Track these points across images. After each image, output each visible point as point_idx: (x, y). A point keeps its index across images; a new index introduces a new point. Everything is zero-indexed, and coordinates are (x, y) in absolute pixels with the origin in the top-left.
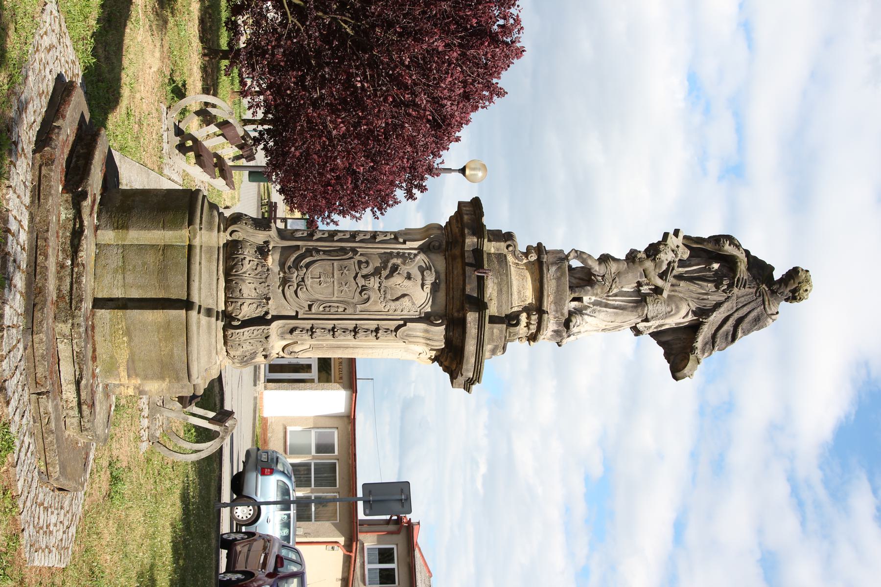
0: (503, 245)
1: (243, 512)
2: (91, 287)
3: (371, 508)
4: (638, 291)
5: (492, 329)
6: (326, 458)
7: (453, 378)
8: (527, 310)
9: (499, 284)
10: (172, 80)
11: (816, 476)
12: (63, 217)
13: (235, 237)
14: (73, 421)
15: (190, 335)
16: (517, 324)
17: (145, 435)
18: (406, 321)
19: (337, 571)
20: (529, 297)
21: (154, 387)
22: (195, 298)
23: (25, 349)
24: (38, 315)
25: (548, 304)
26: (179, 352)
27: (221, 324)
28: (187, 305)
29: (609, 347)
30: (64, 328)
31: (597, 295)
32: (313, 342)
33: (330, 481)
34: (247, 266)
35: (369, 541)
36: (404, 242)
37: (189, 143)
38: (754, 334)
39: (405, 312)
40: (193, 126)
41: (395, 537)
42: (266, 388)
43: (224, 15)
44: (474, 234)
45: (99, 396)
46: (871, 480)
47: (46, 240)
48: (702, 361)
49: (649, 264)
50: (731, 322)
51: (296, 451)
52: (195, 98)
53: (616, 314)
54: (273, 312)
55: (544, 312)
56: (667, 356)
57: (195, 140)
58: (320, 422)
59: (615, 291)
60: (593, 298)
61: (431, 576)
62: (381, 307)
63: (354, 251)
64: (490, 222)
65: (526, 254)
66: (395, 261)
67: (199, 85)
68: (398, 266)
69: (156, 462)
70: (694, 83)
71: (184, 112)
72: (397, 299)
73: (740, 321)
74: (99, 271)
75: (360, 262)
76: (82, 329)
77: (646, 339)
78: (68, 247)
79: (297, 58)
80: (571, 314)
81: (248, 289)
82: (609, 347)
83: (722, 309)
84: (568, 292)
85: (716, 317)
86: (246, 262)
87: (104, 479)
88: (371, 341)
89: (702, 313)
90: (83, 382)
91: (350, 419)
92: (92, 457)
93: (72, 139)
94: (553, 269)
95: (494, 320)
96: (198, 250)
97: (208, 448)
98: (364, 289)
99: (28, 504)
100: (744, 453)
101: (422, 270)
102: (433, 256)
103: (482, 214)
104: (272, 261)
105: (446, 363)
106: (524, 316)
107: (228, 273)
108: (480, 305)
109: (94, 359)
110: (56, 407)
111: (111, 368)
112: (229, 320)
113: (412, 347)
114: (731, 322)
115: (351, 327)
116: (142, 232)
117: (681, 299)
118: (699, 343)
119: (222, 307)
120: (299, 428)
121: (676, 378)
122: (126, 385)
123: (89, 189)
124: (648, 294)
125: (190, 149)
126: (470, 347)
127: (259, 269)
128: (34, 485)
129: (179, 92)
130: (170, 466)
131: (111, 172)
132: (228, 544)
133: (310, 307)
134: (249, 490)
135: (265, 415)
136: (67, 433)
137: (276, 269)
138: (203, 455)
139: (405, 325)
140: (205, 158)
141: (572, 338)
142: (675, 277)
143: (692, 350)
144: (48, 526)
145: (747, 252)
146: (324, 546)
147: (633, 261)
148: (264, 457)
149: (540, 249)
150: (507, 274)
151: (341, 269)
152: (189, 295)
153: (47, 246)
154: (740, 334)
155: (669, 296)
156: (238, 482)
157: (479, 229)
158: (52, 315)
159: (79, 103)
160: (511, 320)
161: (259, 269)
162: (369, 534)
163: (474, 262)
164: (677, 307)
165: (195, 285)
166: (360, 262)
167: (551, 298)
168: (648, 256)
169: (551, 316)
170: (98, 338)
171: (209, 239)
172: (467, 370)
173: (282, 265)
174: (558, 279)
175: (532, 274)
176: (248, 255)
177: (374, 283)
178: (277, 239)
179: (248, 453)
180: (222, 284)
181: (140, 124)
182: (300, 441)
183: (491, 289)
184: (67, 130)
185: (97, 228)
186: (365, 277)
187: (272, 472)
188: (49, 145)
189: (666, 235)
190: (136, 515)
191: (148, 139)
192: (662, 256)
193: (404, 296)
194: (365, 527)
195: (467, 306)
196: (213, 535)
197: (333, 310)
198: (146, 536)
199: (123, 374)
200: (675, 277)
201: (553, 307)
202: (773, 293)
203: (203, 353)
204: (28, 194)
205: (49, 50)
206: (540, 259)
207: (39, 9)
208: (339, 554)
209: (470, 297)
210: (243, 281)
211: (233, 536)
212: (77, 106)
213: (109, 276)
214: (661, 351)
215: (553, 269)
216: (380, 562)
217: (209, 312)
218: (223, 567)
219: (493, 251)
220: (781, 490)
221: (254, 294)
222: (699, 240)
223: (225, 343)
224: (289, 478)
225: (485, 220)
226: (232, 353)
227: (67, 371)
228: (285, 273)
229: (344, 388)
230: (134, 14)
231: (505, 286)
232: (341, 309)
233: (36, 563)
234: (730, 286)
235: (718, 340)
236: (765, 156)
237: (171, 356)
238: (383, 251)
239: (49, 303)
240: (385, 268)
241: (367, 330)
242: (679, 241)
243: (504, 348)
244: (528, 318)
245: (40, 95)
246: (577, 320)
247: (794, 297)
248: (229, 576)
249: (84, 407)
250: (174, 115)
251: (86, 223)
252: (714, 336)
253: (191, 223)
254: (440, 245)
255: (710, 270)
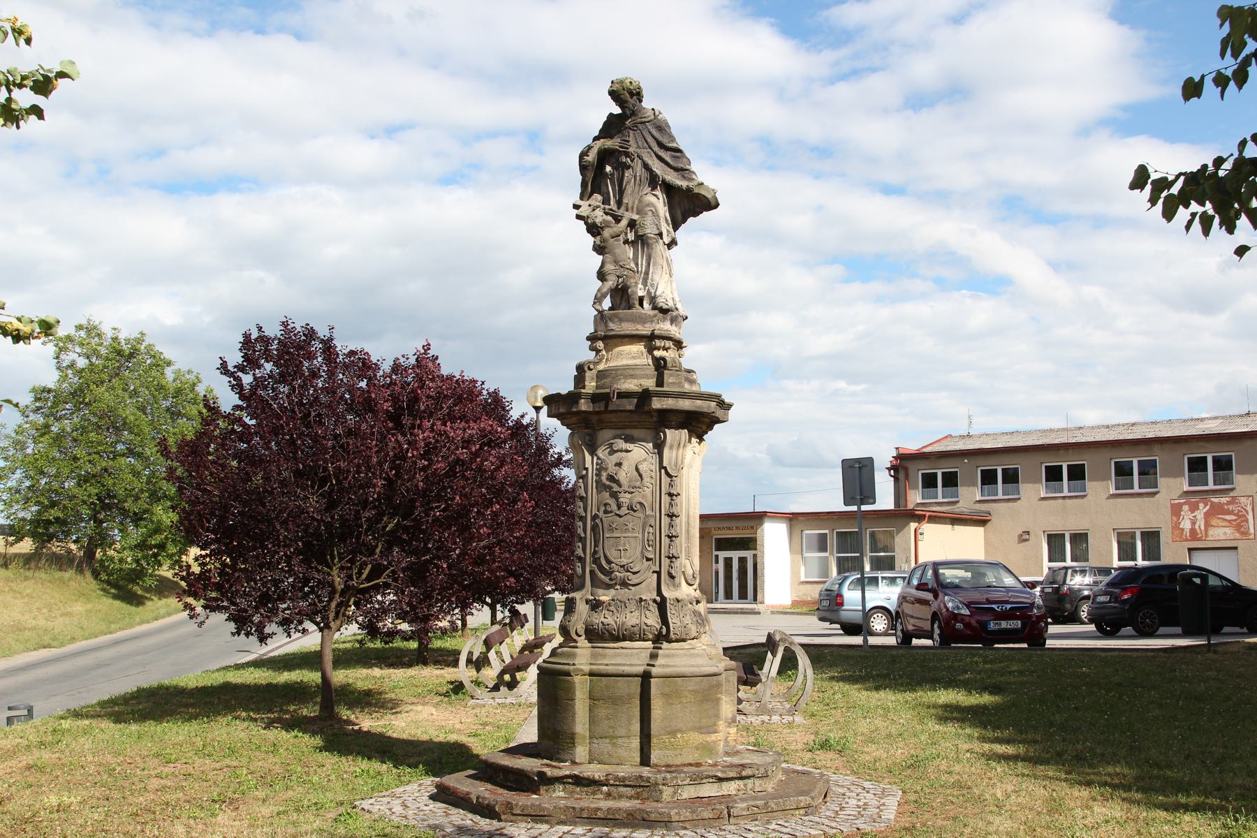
0: (588, 374)
1: (879, 623)
2: (629, 768)
3: (868, 497)
4: (633, 243)
5: (669, 384)
6: (832, 542)
7: (718, 421)
8: (650, 350)
9: (626, 377)
10: (446, 695)
11: (829, 56)
12: (562, 794)
13: (582, 632)
14: (759, 784)
15: (674, 674)
16: (664, 359)
17: (788, 718)
18: (662, 467)
19: (944, 530)
20: (639, 348)
21: (727, 708)
22: (640, 669)
23: (685, 828)
24: (653, 817)
25: (645, 330)
26: (692, 685)
27: (665, 645)
28: (646, 677)
29: (688, 267)
30: (667, 792)
31: (637, 283)
32: (683, 556)
33: (855, 535)
34: (610, 620)
35: (915, 497)
36: (586, 469)
37: (507, 677)
38: (674, 131)
39: (653, 468)
40: (490, 674)
41: (911, 472)
42: (762, 603)
43: (378, 644)
44: (577, 403)
45: (736, 760)
46: (828, 7)
47: (582, 810)
48: (700, 180)
49: (606, 233)
50: (662, 153)
51: (825, 572)
52: (463, 673)
53: (655, 264)
54: (654, 595)
55: (653, 333)
56: (696, 214)
57: (503, 672)
58: (796, 547)
59: (633, 265)
60: (640, 286)
61: (950, 436)
62: (648, 491)
63: (594, 517)
64: (567, 387)
65: (598, 351)
66: (604, 478)
67: (451, 670)
69: (815, 708)
70: (448, 180)
71: (477, 683)
72: (641, 476)
73: (661, 145)
74: (614, 761)
75: (606, 512)
76: (668, 776)
77: (681, 234)
78: (590, 789)
79: (418, 574)
80: (655, 308)
81: (631, 619)
82: (688, 267)
83: (650, 162)
84: (634, 310)
85: (658, 168)
86: (605, 621)
87: (823, 757)
88: (682, 501)
89: (654, 181)
90: (720, 774)
91: (794, 519)
92: (800, 768)
93: (489, 786)
94: (611, 325)
95: (660, 383)
96: (594, 667)
97: (803, 660)
98: (631, 508)
99: (834, 824)
100: (811, 128)
101: (612, 452)
102: (600, 441)
103: (559, 394)
104: (605, 596)
105: (704, 427)
106: (657, 353)
107: (617, 639)
108: (645, 396)
109: (698, 765)
110: (743, 800)
111: (709, 749)
112: (661, 637)
113: (687, 461)
114: (662, 153)
115: (668, 520)
116: (577, 720)
117: (640, 201)
118: (683, 184)
119: (649, 644)
120: (803, 569)
121: (717, 205)
122: (726, 735)
123: (535, 770)
124: (636, 233)
125: (513, 677)
126: (686, 404)
127: (612, 608)
128: (817, 819)
129: (458, 687)
130: (821, 695)
131: (524, 750)
132: (907, 638)
133: (648, 559)
134: (857, 617)
135: (789, 603)
136: (770, 790)
137: (612, 592)
138: (808, 662)
139: (665, 468)
140: (520, 662)
141: (679, 306)
142: (619, 208)
143: (689, 190)
144: (859, 807)
145: (596, 139)
146: (920, 543)
147: (604, 248)
148: (825, 603)
149: (592, 338)
150: (616, 369)
151: (611, 530)
152: (636, 676)
153: (588, 808)
154: (674, 145)
155: (638, 213)
156: (850, 629)
157: (573, 398)
158: (655, 804)
159: (456, 780)
160: (660, 366)
161: (612, 608)
164: (648, 205)
165: (628, 669)
166: (606, 512)
167: (639, 327)
168: (599, 234)
169: (657, 327)
170: (678, 761)
171: (583, 656)
172: (709, 407)
173: (608, 587)
174: (621, 320)
175: (617, 346)
176: (599, 619)
177: (625, 499)
178: (584, 591)
179: (821, 619)
180: (627, 644)
181: (485, 724)
182: (815, 568)
183: (631, 385)
184: (482, 790)
185: (574, 763)
186: (619, 507)
187: (840, 596)
188: (493, 807)
189: (578, 217)
190: (863, 726)
191: (501, 717)
192: (598, 221)
193: (637, 469)
194: (902, 502)
195: (646, 408)
196: (894, 652)
197: (652, 537)
198: (885, 716)
199: (713, 737)
200: (619, 208)
201: (647, 325)
202: (633, 114)
203: (693, 661)
204: (539, 826)
205: (405, 806)
206: (603, 338)
207: (367, 815)
208: (928, 528)
209: (637, 406)
210: (623, 623)
211: (899, 633)
212: (460, 781)
213: (620, 751)
214: (691, 220)
215: (611, 325)
216: (936, 486)
217: (654, 656)
218: (928, 642)
219: (594, 384)
220: (843, 90)
221: (636, 614)
222: (584, 185)
223: (684, 640)
224: (846, 578)
225: (564, 392)
226: (694, 634)
227: (709, 790)
229: (762, 524)
230: (379, 730)
231: (628, 372)
232: (651, 530)
233: (892, 817)
234: (627, 155)
235: (680, 165)
236: (515, 110)
237: (695, 692)
239: (642, 807)
240: (611, 488)
241: (671, 505)
242: (584, 204)
243: (689, 371)
244: (658, 349)
245: (448, 815)
246: (661, 302)
247: (637, 94)
248: (936, 636)
249: (744, 773)
250: (479, 692)
251: (567, 773)
252: (676, 169)
253: (568, 674)
254: (589, 435)
255: (612, 175)
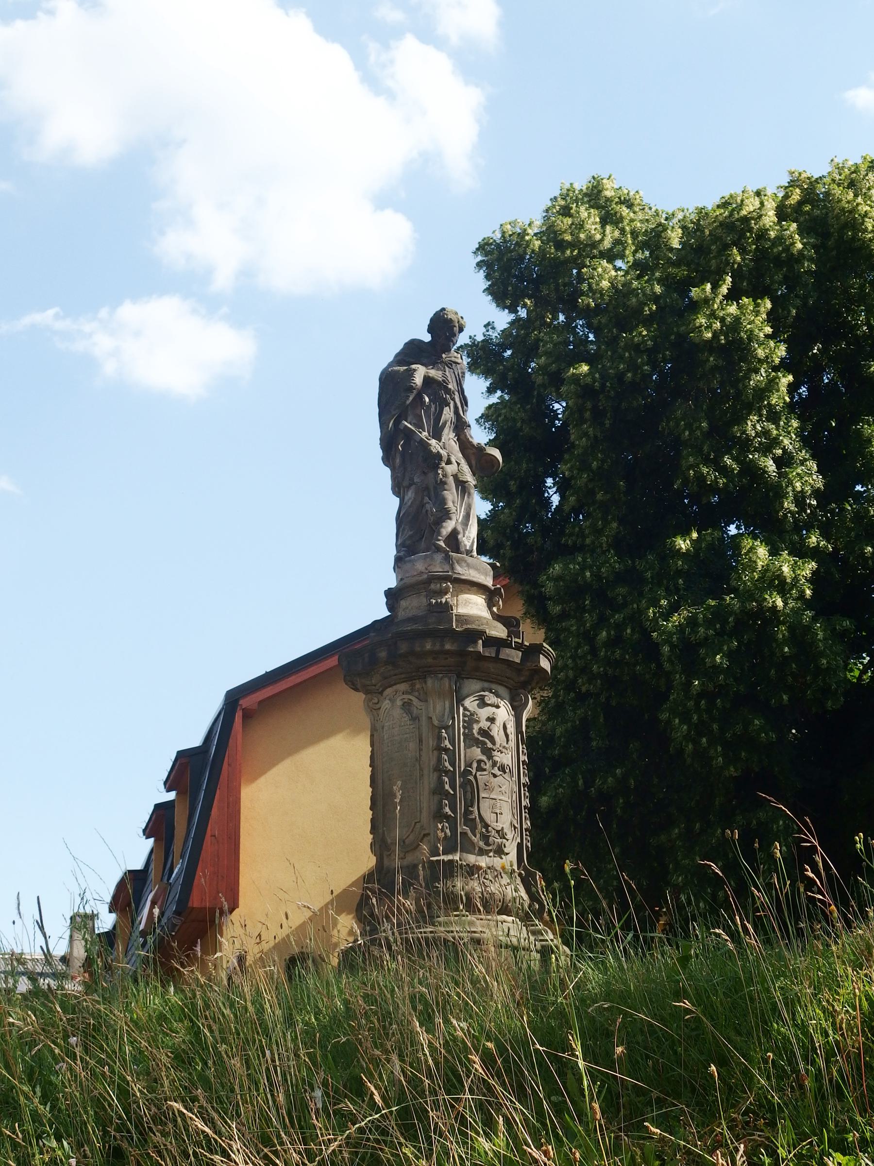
44: (475, 642)
68: (480, 729)
101: (483, 704)
162: (167, 774)
163: (495, 648)
167: (483, 577)
173: (482, 852)
175: (462, 592)
228: (491, 850)
238: (462, 744)
